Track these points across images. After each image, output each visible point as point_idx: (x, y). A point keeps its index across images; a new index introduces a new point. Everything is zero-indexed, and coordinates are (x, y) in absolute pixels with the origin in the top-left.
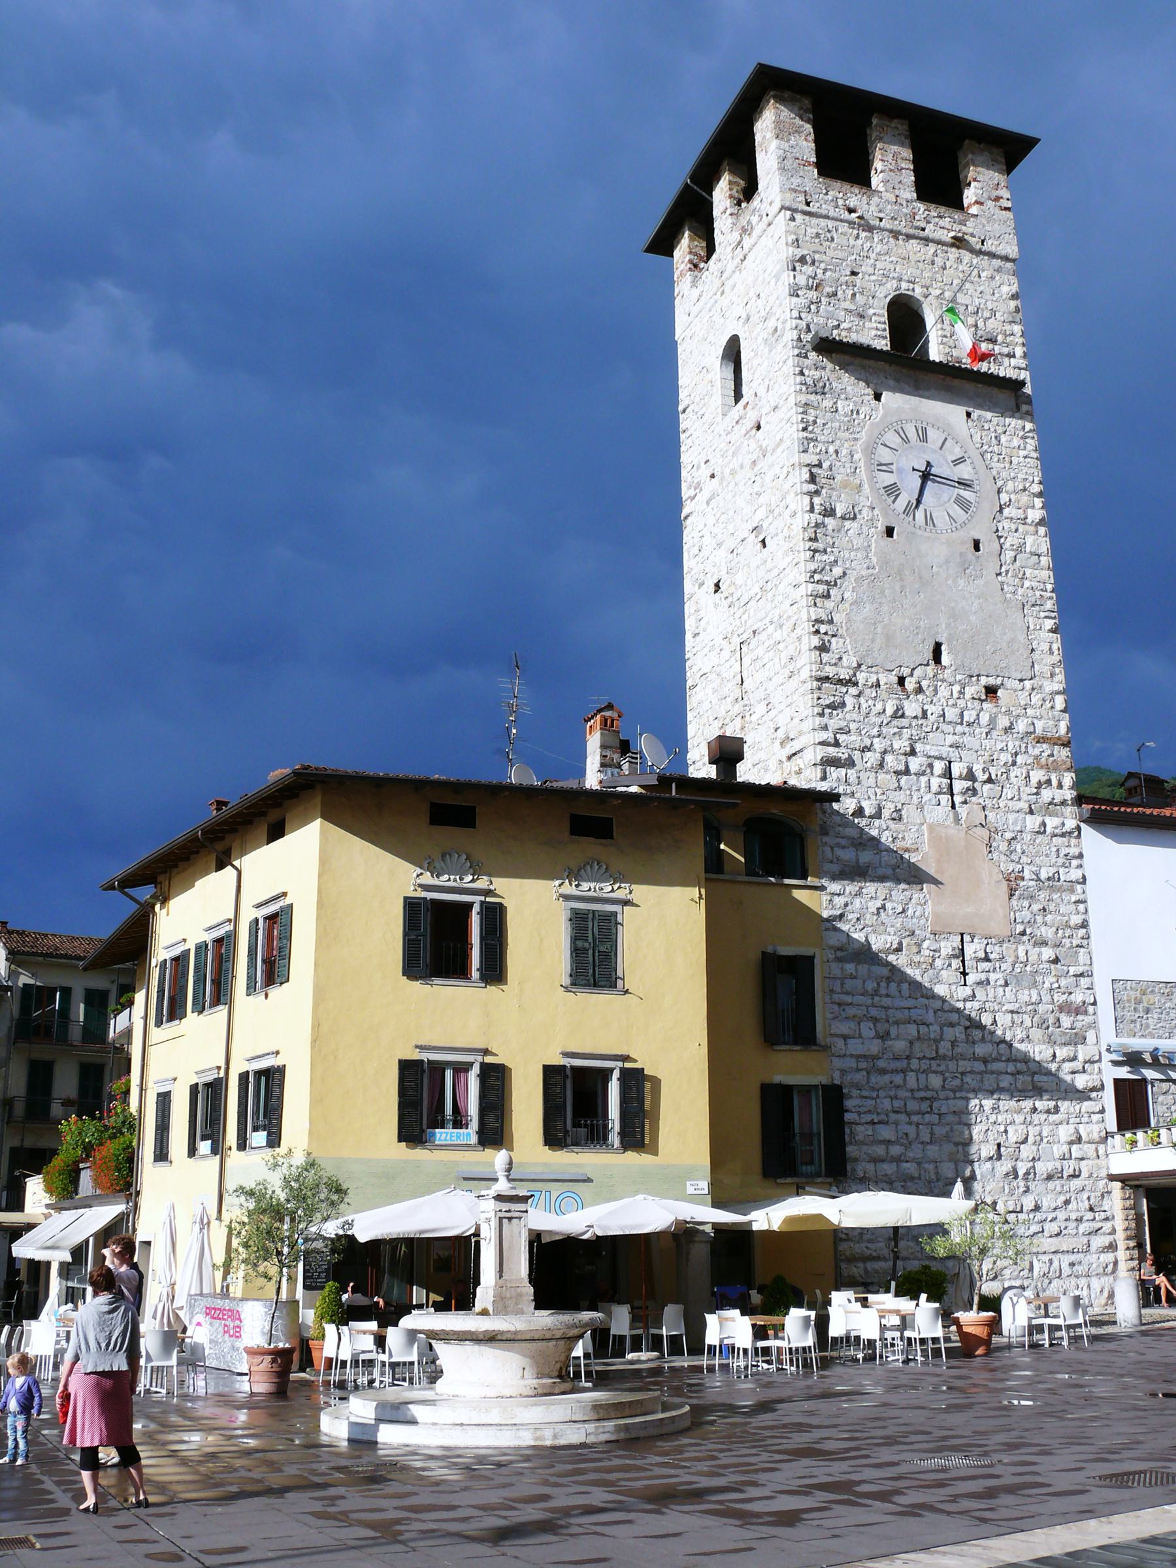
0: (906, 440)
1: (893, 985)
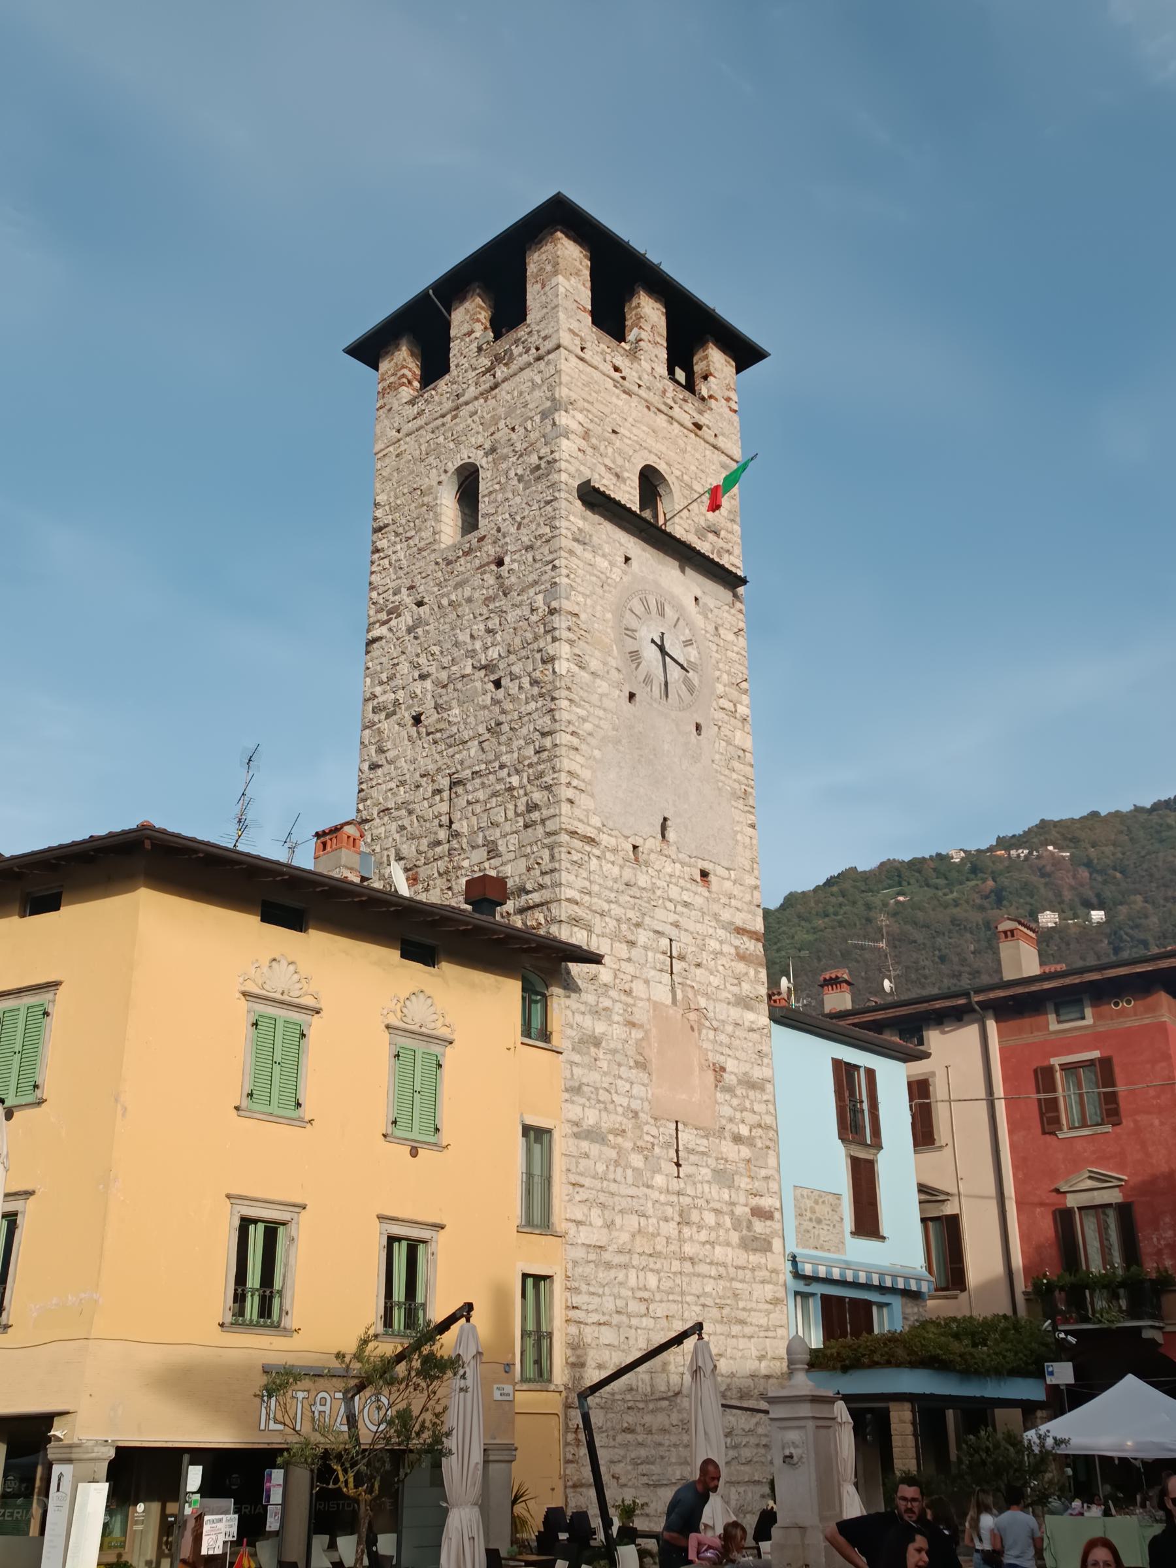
0: (648, 610)
1: (619, 1170)
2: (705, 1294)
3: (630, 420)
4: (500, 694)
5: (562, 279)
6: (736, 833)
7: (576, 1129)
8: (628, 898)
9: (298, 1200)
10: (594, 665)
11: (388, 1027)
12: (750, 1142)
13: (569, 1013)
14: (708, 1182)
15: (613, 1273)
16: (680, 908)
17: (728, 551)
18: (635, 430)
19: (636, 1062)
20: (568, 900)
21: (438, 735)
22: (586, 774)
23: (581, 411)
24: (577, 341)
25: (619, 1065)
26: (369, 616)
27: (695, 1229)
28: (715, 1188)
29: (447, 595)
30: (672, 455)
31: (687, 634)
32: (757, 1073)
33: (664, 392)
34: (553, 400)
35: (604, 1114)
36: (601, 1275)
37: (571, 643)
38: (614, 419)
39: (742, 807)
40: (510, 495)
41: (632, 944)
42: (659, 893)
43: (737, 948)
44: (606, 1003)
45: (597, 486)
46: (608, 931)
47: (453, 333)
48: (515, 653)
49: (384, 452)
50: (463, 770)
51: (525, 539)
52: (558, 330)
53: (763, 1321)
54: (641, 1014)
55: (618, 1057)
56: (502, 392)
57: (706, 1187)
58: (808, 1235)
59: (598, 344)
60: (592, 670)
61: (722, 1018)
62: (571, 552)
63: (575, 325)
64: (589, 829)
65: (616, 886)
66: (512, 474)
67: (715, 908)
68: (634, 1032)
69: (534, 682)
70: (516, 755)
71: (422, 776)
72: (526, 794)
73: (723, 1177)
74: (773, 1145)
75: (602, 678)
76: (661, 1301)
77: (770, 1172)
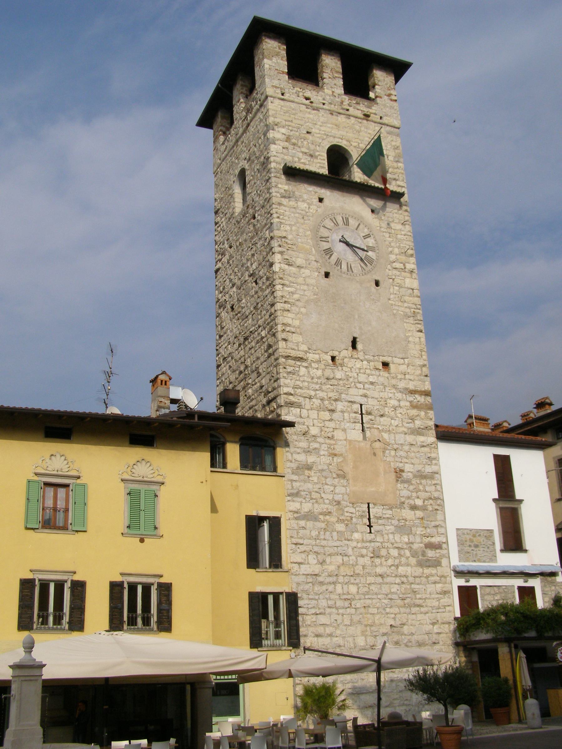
0: (337, 224)
1: (328, 533)
3: (319, 123)
8: (329, 386)
12: (424, 508)
14: (392, 533)
15: (324, 588)
16: (367, 386)
17: (395, 179)
18: (322, 128)
19: (338, 475)
20: (286, 394)
23: (283, 127)
25: (326, 478)
27: (383, 559)
28: (397, 537)
30: (350, 135)
31: (366, 232)
33: (342, 103)
36: (316, 589)
37: (281, 253)
38: (308, 126)
44: (316, 445)
45: (290, 165)
46: (314, 406)
53: (436, 604)
55: (324, 474)
57: (391, 536)
58: (468, 555)
60: (298, 265)
62: (280, 204)
63: (276, 82)
64: (300, 353)
65: (319, 381)
67: (394, 382)
68: (335, 459)
76: (360, 599)
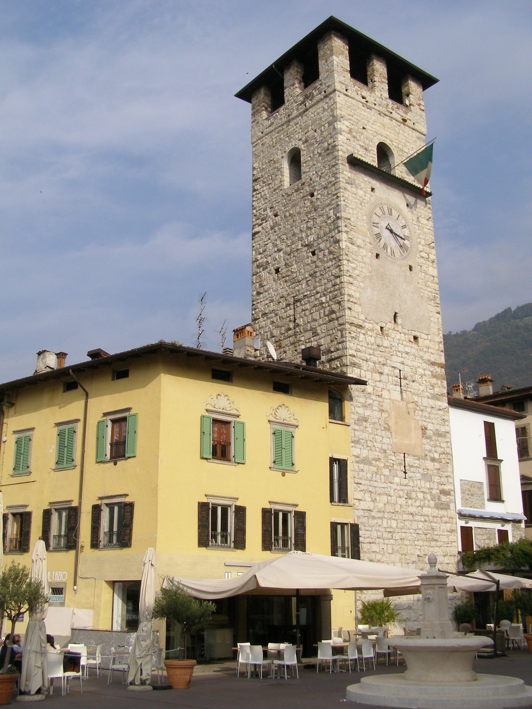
0: (384, 213)
1: (378, 476)
2: (419, 529)
3: (371, 121)
4: (315, 258)
5: (337, 58)
6: (430, 317)
7: (357, 459)
9: (235, 496)
10: (359, 242)
11: (269, 421)
13: (352, 407)
14: (419, 479)
15: (376, 521)
16: (404, 355)
20: (350, 355)
21: (287, 278)
22: (357, 295)
23: (347, 120)
24: (344, 87)
25: (377, 429)
26: (253, 222)
28: (423, 482)
29: (289, 211)
30: (392, 136)
31: (404, 223)
32: (443, 429)
33: (387, 105)
34: (333, 116)
35: (370, 452)
36: (370, 522)
37: (347, 232)
39: (433, 304)
40: (316, 163)
41: (381, 373)
42: (394, 348)
43: (432, 372)
44: (370, 401)
46: (370, 368)
47: (285, 85)
48: (321, 238)
49: (256, 143)
50: (300, 294)
51: (323, 183)
52: (334, 83)
53: (446, 540)
54: (386, 405)
55: (376, 426)
56: (309, 113)
57: (419, 482)
59: (355, 88)
61: (425, 405)
63: (342, 79)
64: (359, 321)
65: (373, 347)
66: (316, 152)
67: (421, 353)
69: (331, 253)
70: (323, 287)
71: (281, 297)
72: (329, 306)
73: (427, 477)
74: (449, 462)
75: (363, 248)
77: (448, 474)
